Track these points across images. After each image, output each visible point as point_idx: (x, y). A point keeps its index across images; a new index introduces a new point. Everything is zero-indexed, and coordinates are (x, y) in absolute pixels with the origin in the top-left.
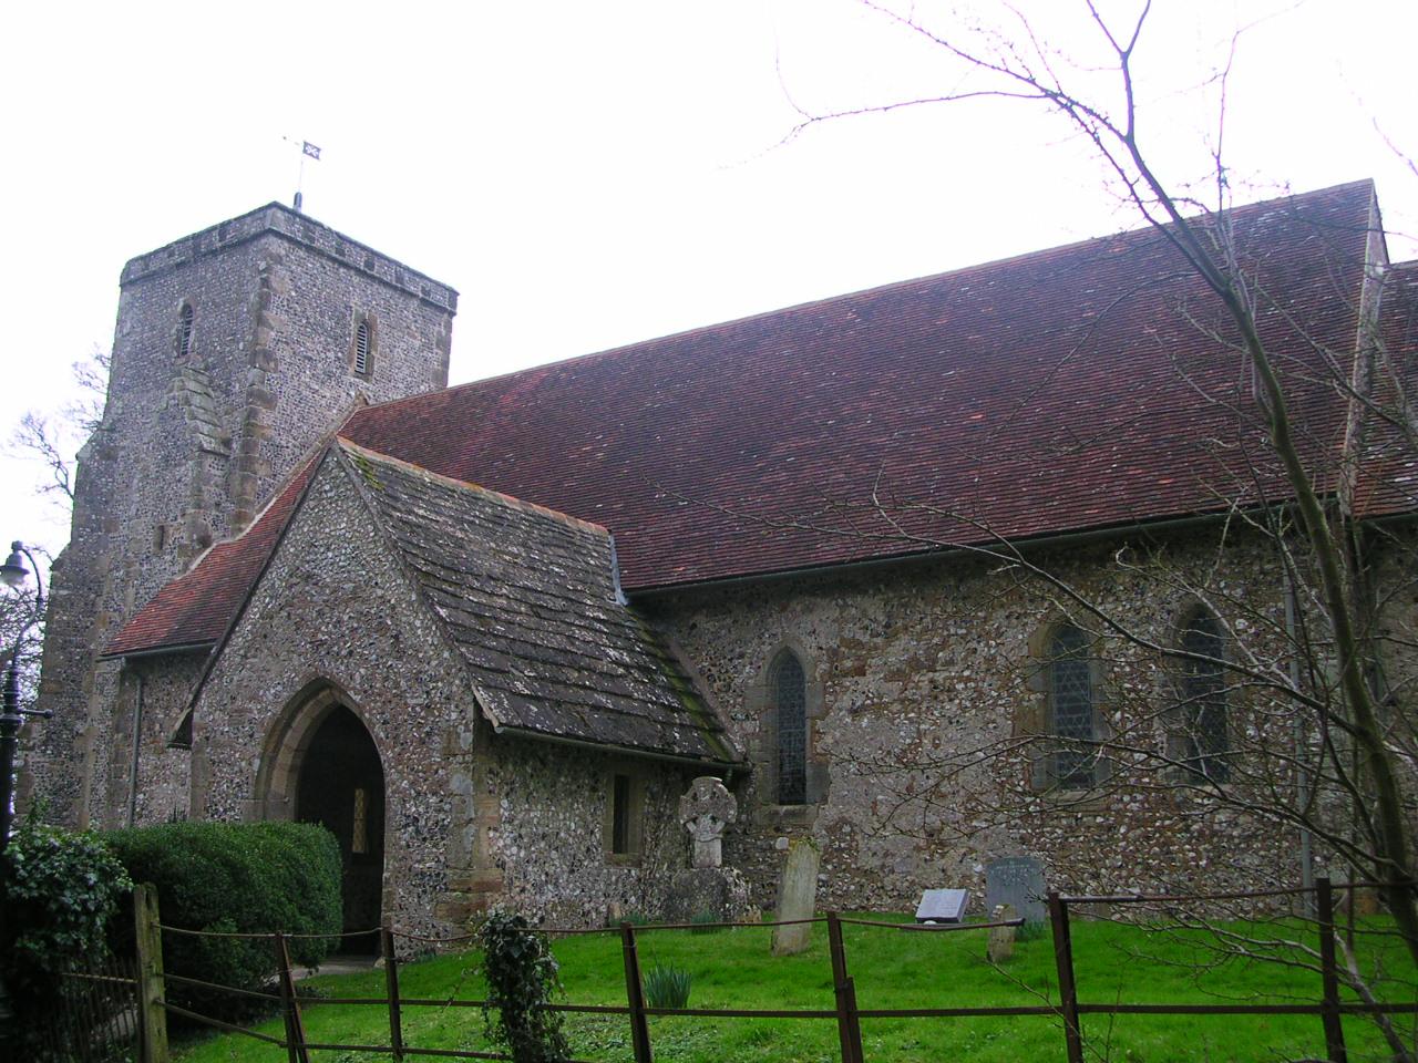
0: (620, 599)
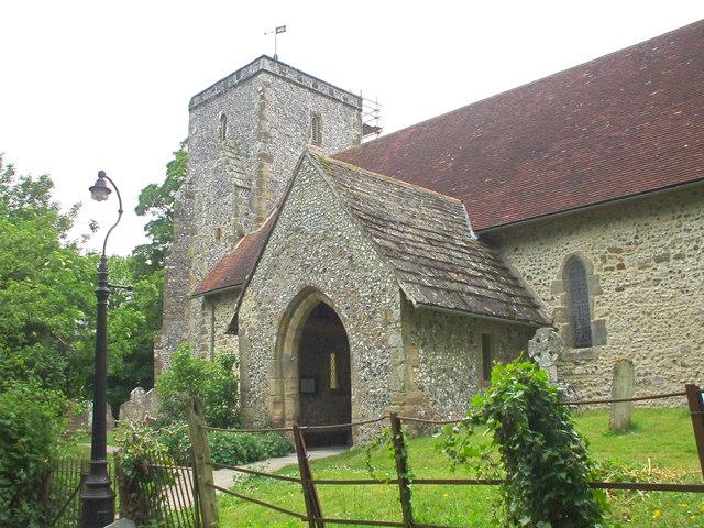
0: (473, 236)
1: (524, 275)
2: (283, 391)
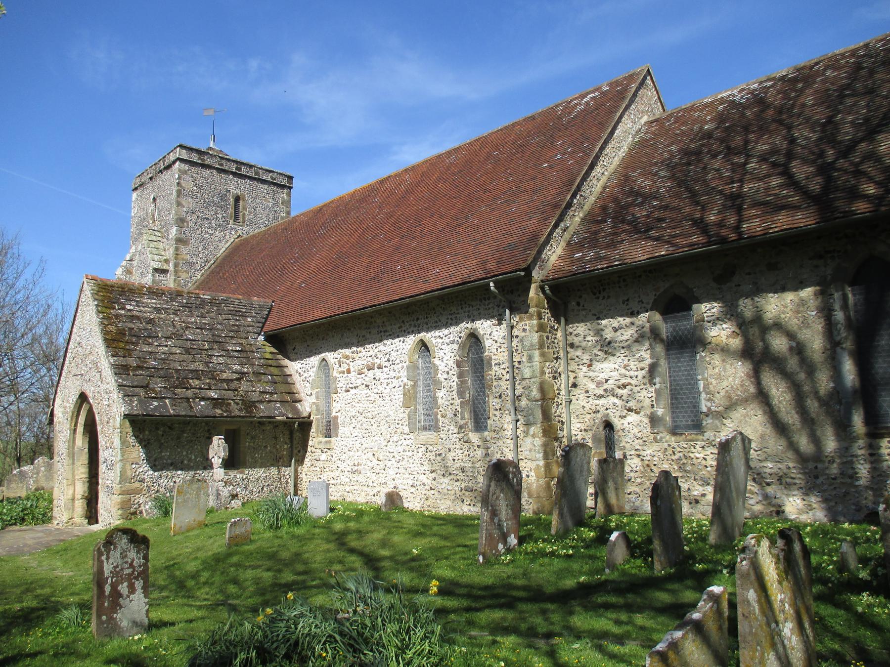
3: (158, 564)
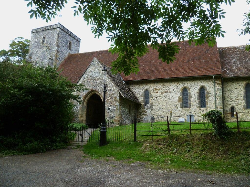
1: (134, 92)
2: (83, 114)
3: (240, 130)
